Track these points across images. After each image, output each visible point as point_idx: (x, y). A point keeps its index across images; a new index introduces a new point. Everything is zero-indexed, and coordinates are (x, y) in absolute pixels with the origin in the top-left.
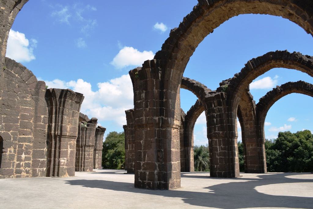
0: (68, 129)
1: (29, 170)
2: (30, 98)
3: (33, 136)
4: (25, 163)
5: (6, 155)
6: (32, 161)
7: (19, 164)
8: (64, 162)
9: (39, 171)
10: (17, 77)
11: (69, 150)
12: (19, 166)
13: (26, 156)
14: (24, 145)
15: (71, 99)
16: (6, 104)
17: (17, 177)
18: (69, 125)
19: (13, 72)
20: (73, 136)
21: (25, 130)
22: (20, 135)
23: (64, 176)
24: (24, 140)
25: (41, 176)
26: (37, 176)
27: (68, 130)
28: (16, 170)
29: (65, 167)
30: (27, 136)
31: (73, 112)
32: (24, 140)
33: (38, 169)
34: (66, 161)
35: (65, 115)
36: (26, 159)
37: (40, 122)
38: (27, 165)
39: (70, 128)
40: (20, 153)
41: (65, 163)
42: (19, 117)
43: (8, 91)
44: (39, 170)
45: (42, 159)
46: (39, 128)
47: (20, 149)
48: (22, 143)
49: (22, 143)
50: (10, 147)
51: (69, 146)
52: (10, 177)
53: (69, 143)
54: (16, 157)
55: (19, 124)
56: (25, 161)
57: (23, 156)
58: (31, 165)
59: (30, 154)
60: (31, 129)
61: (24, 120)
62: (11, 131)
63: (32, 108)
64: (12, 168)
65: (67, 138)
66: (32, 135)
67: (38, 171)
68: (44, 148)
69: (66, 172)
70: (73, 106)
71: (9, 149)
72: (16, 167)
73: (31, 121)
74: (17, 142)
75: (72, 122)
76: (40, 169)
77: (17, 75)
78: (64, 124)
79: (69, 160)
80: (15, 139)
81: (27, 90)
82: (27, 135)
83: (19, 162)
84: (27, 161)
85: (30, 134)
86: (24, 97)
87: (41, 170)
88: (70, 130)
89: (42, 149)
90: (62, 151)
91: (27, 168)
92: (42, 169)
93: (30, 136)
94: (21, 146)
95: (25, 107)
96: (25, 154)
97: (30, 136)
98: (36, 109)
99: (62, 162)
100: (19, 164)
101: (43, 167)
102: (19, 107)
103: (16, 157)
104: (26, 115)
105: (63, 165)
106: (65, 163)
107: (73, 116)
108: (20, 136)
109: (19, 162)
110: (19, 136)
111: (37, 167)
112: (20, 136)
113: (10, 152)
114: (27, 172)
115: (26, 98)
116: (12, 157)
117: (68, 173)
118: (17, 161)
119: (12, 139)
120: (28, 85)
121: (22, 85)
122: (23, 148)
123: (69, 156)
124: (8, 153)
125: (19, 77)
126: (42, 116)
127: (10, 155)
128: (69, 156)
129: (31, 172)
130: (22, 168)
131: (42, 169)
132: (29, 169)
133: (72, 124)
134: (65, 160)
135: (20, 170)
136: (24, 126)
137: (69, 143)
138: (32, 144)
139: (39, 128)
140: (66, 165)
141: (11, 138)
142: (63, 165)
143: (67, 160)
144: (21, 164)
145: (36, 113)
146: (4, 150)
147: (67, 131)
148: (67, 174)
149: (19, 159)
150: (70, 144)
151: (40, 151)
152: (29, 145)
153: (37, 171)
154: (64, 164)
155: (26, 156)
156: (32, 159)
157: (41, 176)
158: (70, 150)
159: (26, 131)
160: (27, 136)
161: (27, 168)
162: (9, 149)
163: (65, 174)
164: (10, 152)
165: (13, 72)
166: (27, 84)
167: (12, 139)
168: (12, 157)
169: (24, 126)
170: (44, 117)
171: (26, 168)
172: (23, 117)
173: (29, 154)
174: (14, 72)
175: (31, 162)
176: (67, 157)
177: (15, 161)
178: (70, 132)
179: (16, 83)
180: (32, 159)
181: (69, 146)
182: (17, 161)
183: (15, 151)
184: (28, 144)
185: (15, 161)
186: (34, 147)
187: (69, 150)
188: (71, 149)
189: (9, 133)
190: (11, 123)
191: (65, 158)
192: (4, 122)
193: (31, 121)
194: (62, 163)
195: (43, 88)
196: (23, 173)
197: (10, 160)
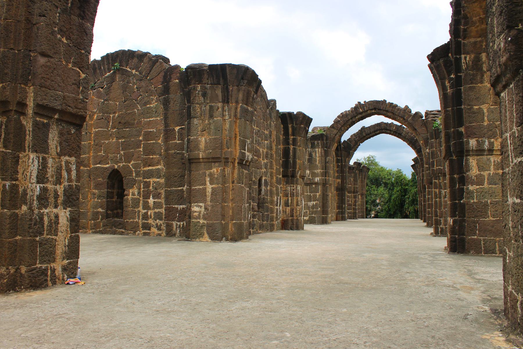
0: (202, 145)
1: (161, 225)
2: (156, 102)
3: (164, 166)
4: (155, 213)
5: (128, 199)
6: (165, 210)
7: (146, 213)
8: (200, 212)
9: (177, 228)
10: (135, 75)
11: (209, 188)
12: (146, 217)
13: (156, 200)
14: (152, 183)
15: (200, 82)
16: (123, 121)
17: (145, 234)
18: (202, 136)
19: (129, 69)
20: (213, 158)
21: (151, 157)
22: (145, 166)
23: (201, 239)
24: (150, 174)
25: (277, 230)
26: (174, 235)
27: (201, 146)
28: (143, 224)
29: (201, 221)
30: (154, 168)
31: (211, 107)
32: (150, 174)
33: (174, 223)
34: (203, 210)
35: (194, 118)
36: (157, 205)
37: (174, 140)
38: (158, 216)
39: (206, 141)
40: (146, 196)
41: (202, 213)
42: (141, 138)
43: (125, 101)
44: (177, 225)
45: (181, 206)
46: (173, 151)
47: (146, 189)
48: (148, 180)
49: (148, 180)
50: (132, 187)
51: (208, 179)
52: (135, 235)
53: (208, 172)
54: (141, 202)
55: (141, 149)
56: (154, 208)
57: (151, 201)
58: (164, 217)
59: (161, 197)
60: (160, 155)
61: (149, 141)
62: (132, 162)
63: (159, 119)
64: (137, 220)
65: (203, 164)
66: (162, 164)
67: (175, 227)
68: (184, 186)
69: (205, 232)
70: (209, 96)
71: (131, 191)
72: (143, 219)
73: (160, 141)
74: (141, 178)
75: (209, 128)
76: (178, 223)
77: (134, 71)
78: (85, 153)
79: (210, 208)
80: (138, 175)
81: (150, 90)
82: (153, 166)
83: (146, 211)
84: (157, 208)
85: (158, 163)
86: (146, 104)
87: (180, 226)
88: (205, 147)
89: (179, 188)
90: (194, 190)
91: (158, 221)
92: (182, 223)
93: (159, 167)
94: (147, 185)
95: (148, 120)
96: (153, 198)
97: (159, 167)
98: (166, 118)
99: (195, 212)
100: (146, 213)
101: (183, 221)
102: (141, 121)
103: (141, 202)
104: (151, 131)
105: (198, 217)
106: (202, 213)
107: (211, 116)
108: (145, 169)
109: (146, 211)
110: (143, 168)
111: (173, 220)
112: (145, 169)
113: (133, 194)
114: (159, 228)
115: (150, 104)
116: (136, 203)
117: (208, 233)
118: (144, 209)
119: (134, 175)
120: (151, 81)
121: (143, 84)
122: (151, 188)
123: (209, 199)
124: (130, 197)
125: (137, 73)
126: (177, 129)
127: (133, 199)
128: (209, 199)
129: (163, 227)
130: (150, 221)
131: (182, 223)
132: (161, 222)
133: (209, 134)
134: (201, 207)
135: (148, 223)
136: (149, 151)
137: (208, 172)
138: (162, 181)
139: (173, 151)
140: (205, 219)
141: (133, 174)
142: (198, 217)
143: (206, 209)
144: (149, 213)
145: (166, 125)
146: (126, 192)
147: (199, 150)
148: (206, 235)
149: (146, 206)
150: (211, 175)
151: (176, 191)
152: (158, 181)
153: (173, 227)
154: (199, 215)
155: (156, 200)
156: (164, 206)
157: (180, 235)
158: (211, 187)
159: (153, 158)
160: (154, 168)
161: (158, 221)
162: (131, 191)
163: (201, 235)
164: (133, 194)
165: (129, 69)
166: (149, 80)
167: (134, 175)
168: (136, 203)
169: (149, 151)
170: (181, 128)
171: (156, 220)
172: (148, 136)
173: (159, 198)
174: (130, 69)
175: (163, 211)
176: (205, 201)
177: (141, 208)
178: (204, 151)
179: (134, 84)
180: (164, 206)
181: (208, 179)
182: (144, 209)
183: (139, 193)
184: (158, 180)
185: (141, 208)
186: (168, 184)
187: (209, 188)
188: (213, 186)
189: (130, 165)
190: (132, 149)
191: (201, 204)
192: (123, 150)
193: (160, 141)
194: (196, 214)
195: (175, 77)
196: (154, 230)
197: (134, 208)
